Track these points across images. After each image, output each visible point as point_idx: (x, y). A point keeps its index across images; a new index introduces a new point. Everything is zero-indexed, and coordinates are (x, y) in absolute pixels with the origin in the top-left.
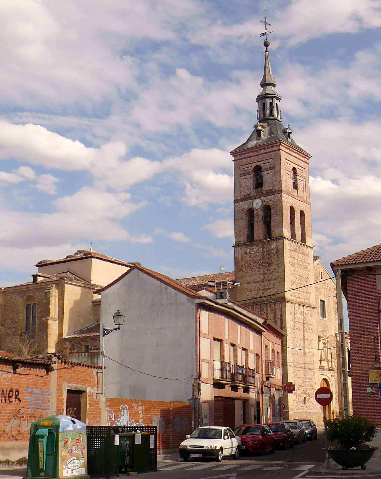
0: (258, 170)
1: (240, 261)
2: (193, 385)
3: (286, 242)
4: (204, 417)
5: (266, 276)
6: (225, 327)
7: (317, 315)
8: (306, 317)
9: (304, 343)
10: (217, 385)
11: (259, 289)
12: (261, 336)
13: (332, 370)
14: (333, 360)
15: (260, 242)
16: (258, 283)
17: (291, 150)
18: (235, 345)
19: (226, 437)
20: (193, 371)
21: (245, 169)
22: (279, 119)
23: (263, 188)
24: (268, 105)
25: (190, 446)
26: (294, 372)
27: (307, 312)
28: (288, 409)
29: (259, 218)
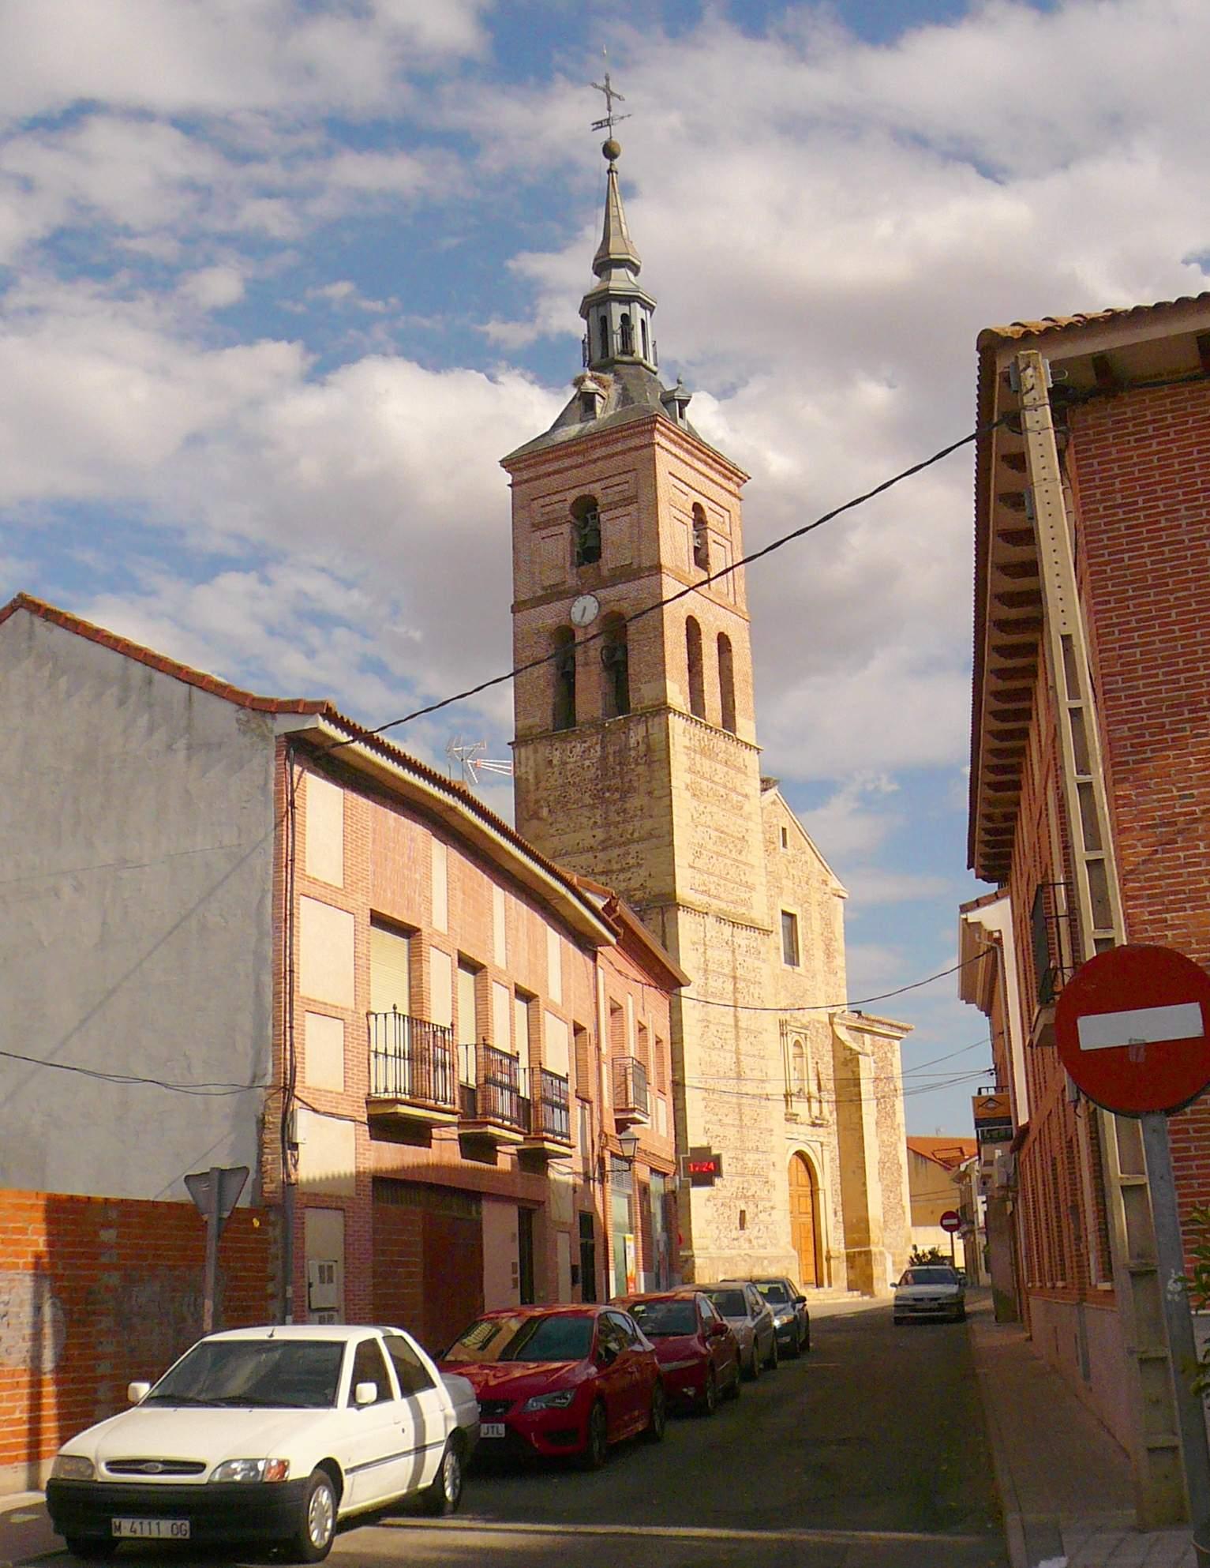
0: (586, 511)
1: (532, 788)
2: (262, 1124)
3: (676, 724)
4: (314, 1276)
5: (613, 831)
6: (428, 877)
7: (773, 952)
8: (740, 959)
9: (737, 1038)
10: (386, 1124)
11: (593, 873)
12: (595, 960)
13: (821, 1126)
14: (825, 1096)
15: (597, 726)
16: (590, 855)
17: (687, 451)
18: (484, 967)
19: (368, 1391)
20: (258, 1053)
21: (547, 509)
22: (650, 364)
23: (602, 562)
24: (616, 323)
25: (115, 1465)
26: (706, 1131)
27: (743, 943)
28: (690, 1248)
29: (592, 653)
